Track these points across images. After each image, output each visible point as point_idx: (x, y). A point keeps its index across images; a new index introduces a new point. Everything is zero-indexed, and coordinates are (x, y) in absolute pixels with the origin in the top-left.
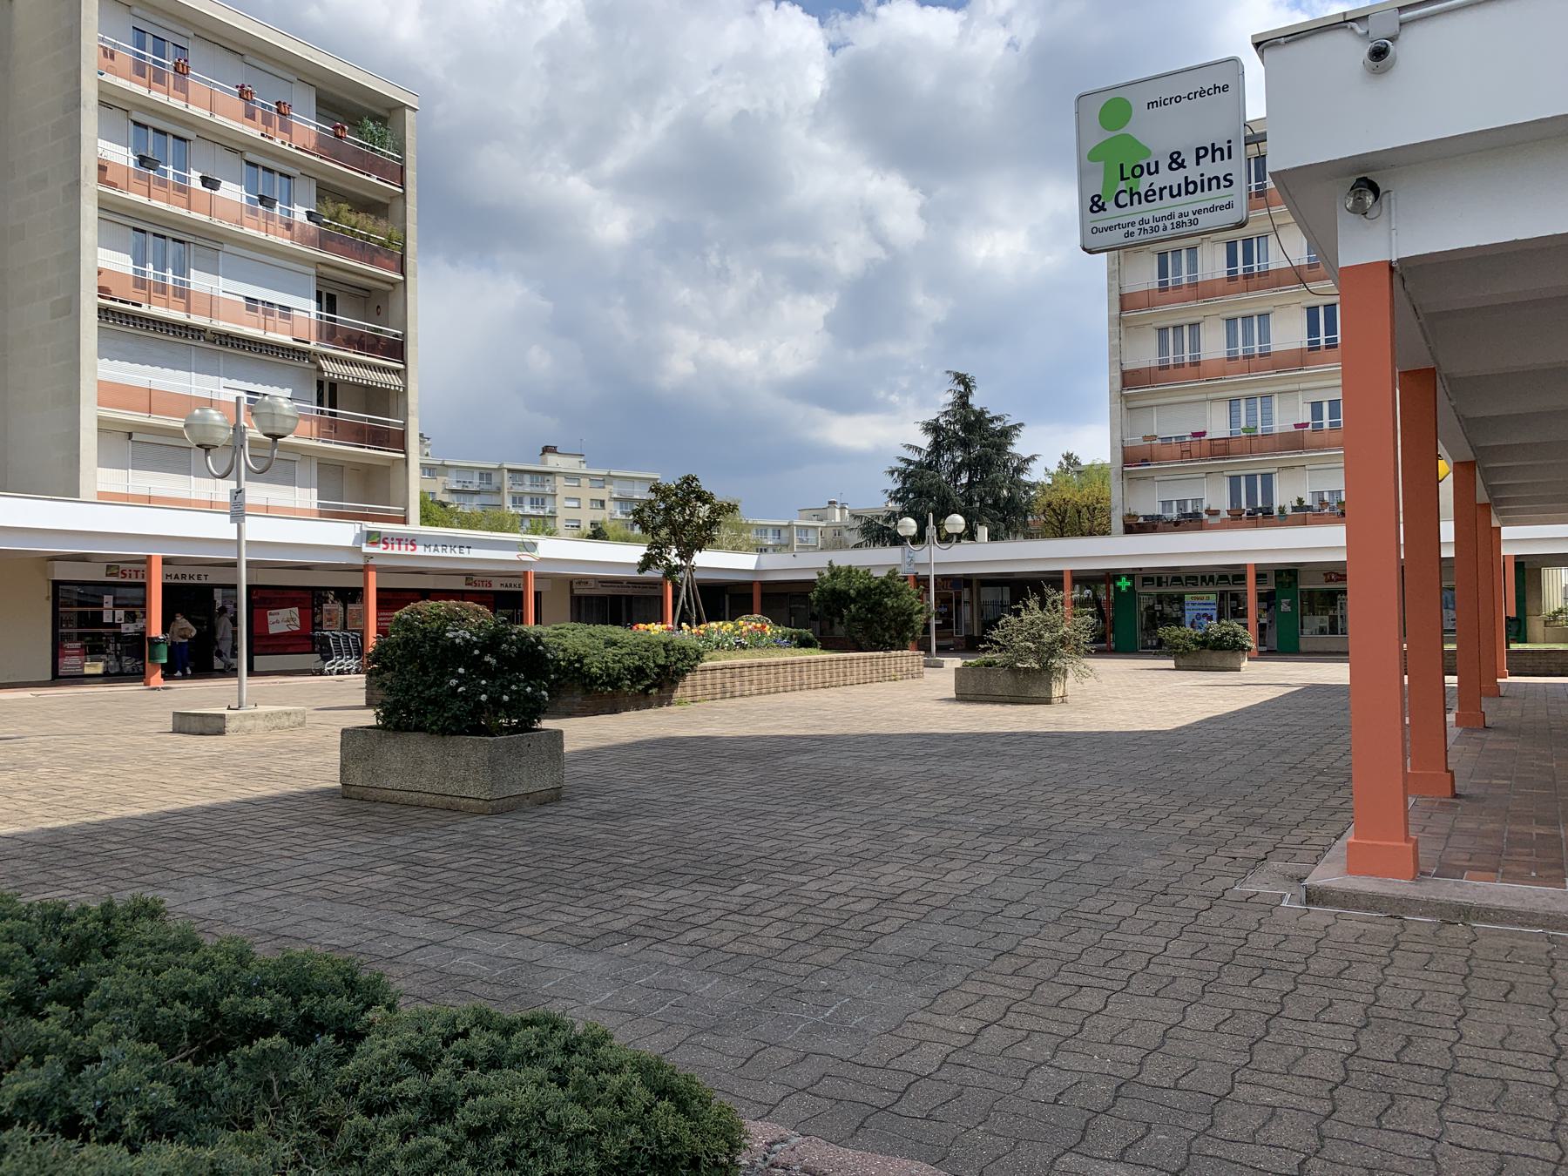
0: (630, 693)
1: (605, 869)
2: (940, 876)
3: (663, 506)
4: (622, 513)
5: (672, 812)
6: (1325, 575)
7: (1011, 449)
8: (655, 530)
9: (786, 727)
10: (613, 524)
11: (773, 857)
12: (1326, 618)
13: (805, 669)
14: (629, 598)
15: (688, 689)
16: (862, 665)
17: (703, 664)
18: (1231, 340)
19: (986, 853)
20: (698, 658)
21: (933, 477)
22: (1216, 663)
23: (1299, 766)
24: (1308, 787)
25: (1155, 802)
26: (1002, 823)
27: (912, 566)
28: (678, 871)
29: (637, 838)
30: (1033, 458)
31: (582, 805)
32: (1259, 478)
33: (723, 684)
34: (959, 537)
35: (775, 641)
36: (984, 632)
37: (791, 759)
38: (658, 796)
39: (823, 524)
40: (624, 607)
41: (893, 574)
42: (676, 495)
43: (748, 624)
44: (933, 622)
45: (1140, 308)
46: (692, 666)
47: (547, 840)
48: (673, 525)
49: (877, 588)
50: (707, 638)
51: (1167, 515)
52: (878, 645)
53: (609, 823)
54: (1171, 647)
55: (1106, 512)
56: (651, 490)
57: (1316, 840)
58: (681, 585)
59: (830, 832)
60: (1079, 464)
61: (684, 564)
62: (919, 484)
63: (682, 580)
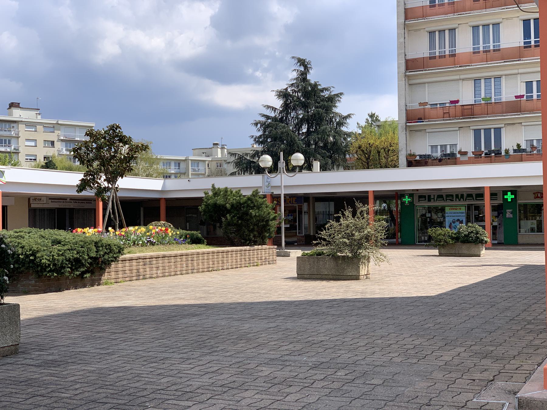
0: (70, 277)
1: (47, 401)
2: (282, 398)
3: (95, 145)
4: (67, 150)
5: (98, 360)
6: (534, 193)
7: (335, 110)
8: (90, 162)
9: (181, 299)
10: (60, 158)
11: (168, 389)
12: (535, 222)
13: (195, 259)
14: (71, 210)
15: (113, 273)
16: (234, 255)
17: (123, 256)
18: (476, 41)
19: (313, 381)
20: (119, 252)
21: (284, 127)
22: (465, 252)
23: (516, 318)
24: (522, 333)
25: (424, 344)
26: (324, 360)
27: (270, 187)
28: (101, 401)
29: (73, 378)
30: (349, 116)
31: (33, 356)
32: (492, 131)
33: (138, 270)
34: (301, 168)
35: (175, 240)
36: (317, 233)
37: (184, 321)
38: (89, 349)
39: (209, 159)
40: (67, 218)
41: (256, 193)
42: (105, 138)
43: (155, 228)
44: (283, 226)
45: (417, 18)
46: (115, 258)
47: (7, 382)
48: (102, 159)
49: (245, 202)
50: (126, 237)
51: (434, 155)
52: (246, 242)
53: (53, 368)
54: (436, 241)
55: (396, 152)
56: (87, 134)
57: (526, 367)
58: (108, 201)
59: (209, 370)
60: (379, 121)
61: (110, 186)
62: (274, 132)
63: (109, 197)
